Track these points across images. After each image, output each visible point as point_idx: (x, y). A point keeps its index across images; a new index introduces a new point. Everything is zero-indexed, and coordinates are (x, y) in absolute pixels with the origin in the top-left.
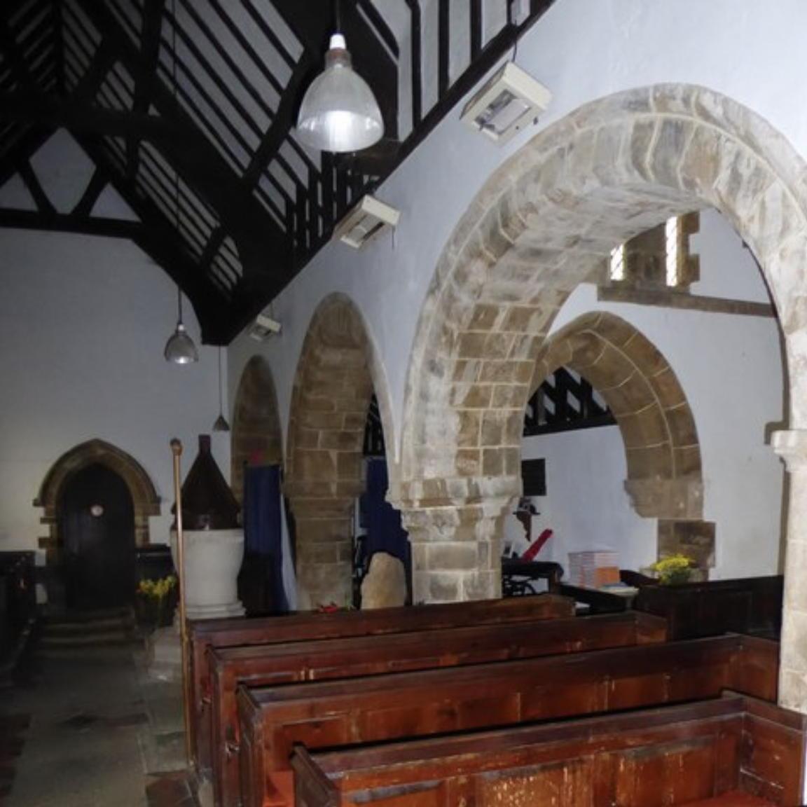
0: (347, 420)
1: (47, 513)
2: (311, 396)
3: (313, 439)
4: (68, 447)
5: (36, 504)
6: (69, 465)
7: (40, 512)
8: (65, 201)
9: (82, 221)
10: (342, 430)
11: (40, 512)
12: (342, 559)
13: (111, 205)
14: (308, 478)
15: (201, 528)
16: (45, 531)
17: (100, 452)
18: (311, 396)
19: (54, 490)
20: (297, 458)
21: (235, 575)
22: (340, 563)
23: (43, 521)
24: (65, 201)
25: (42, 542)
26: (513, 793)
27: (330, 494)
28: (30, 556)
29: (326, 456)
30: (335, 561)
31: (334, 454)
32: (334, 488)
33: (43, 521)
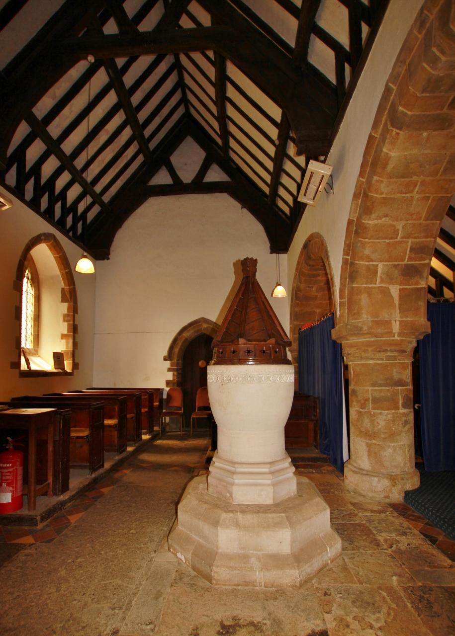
0: (412, 249)
1: (172, 365)
2: (370, 222)
3: (372, 272)
4: (185, 323)
5: (165, 359)
6: (186, 335)
7: (168, 364)
8: (187, 176)
9: (199, 186)
10: (406, 262)
11: (168, 364)
12: (404, 406)
13: (215, 175)
14: (365, 318)
15: (241, 361)
16: (170, 376)
17: (205, 326)
18: (370, 222)
19: (176, 350)
20: (351, 303)
21: (218, 427)
22: (402, 411)
23: (169, 370)
24: (187, 176)
25: (168, 383)
26: (423, 502)
27: (391, 333)
28: (159, 391)
29: (386, 292)
30: (397, 408)
31: (395, 290)
32: (396, 327)
33: (169, 370)
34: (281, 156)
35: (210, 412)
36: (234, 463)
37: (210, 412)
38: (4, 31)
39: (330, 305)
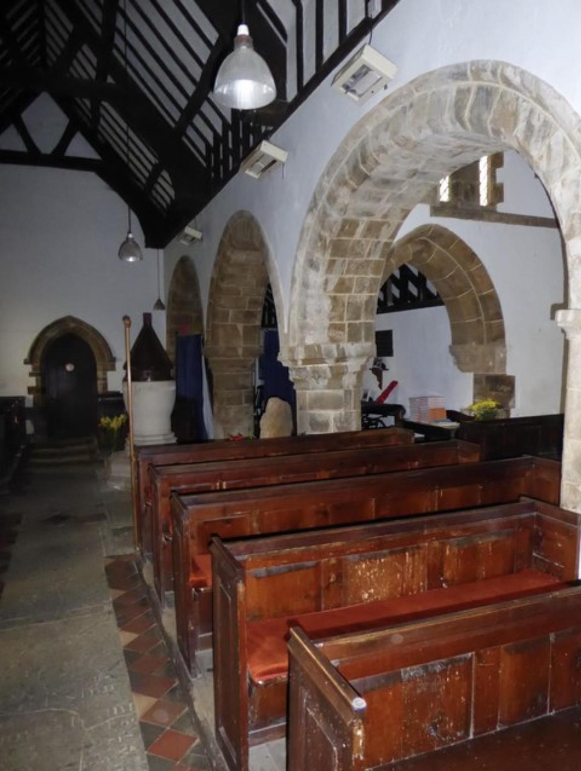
0: (250, 302)
1: (34, 369)
2: (224, 285)
3: (225, 316)
4: (49, 322)
5: (26, 362)
6: (50, 335)
7: (29, 368)
8: (47, 144)
9: (59, 159)
10: (247, 309)
11: (29, 368)
12: (246, 402)
13: (80, 147)
14: (222, 344)
16: (33, 382)
17: (72, 325)
18: (224, 285)
19: (39, 353)
20: (214, 329)
22: (245, 405)
23: (31, 375)
24: (47, 144)
25: (30, 390)
27: (237, 356)
28: (21, 400)
29: (235, 328)
30: (241, 403)
31: (240, 327)
32: (240, 351)
33: (31, 375)
34: (125, 27)
35: (274, 329)
36: (143, 436)
37: (274, 329)
38: (3, 135)
39: (227, 749)
